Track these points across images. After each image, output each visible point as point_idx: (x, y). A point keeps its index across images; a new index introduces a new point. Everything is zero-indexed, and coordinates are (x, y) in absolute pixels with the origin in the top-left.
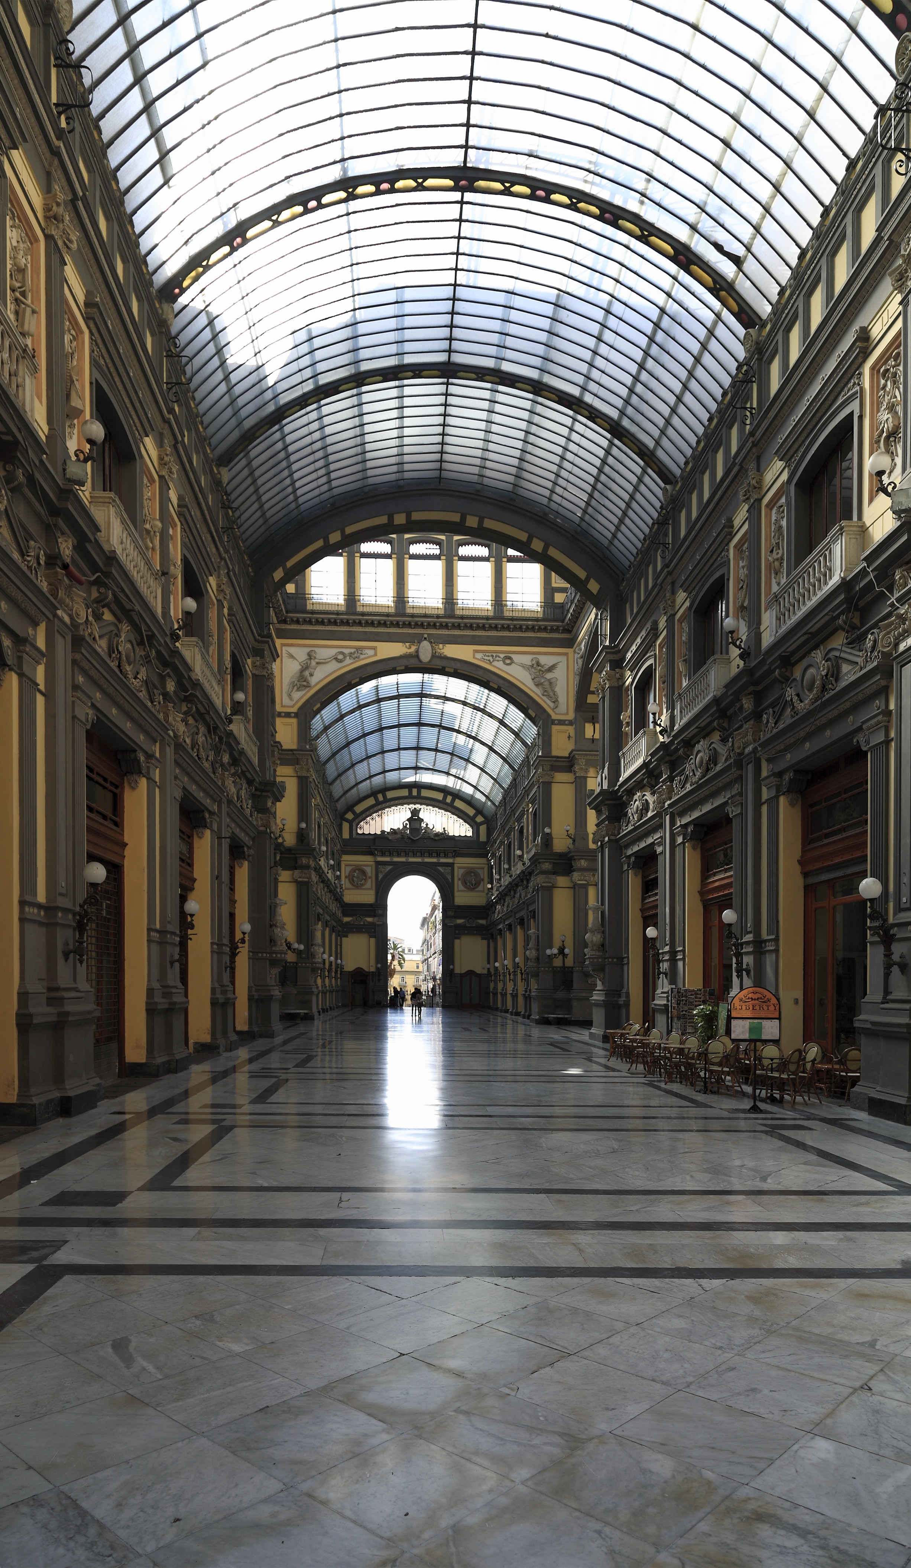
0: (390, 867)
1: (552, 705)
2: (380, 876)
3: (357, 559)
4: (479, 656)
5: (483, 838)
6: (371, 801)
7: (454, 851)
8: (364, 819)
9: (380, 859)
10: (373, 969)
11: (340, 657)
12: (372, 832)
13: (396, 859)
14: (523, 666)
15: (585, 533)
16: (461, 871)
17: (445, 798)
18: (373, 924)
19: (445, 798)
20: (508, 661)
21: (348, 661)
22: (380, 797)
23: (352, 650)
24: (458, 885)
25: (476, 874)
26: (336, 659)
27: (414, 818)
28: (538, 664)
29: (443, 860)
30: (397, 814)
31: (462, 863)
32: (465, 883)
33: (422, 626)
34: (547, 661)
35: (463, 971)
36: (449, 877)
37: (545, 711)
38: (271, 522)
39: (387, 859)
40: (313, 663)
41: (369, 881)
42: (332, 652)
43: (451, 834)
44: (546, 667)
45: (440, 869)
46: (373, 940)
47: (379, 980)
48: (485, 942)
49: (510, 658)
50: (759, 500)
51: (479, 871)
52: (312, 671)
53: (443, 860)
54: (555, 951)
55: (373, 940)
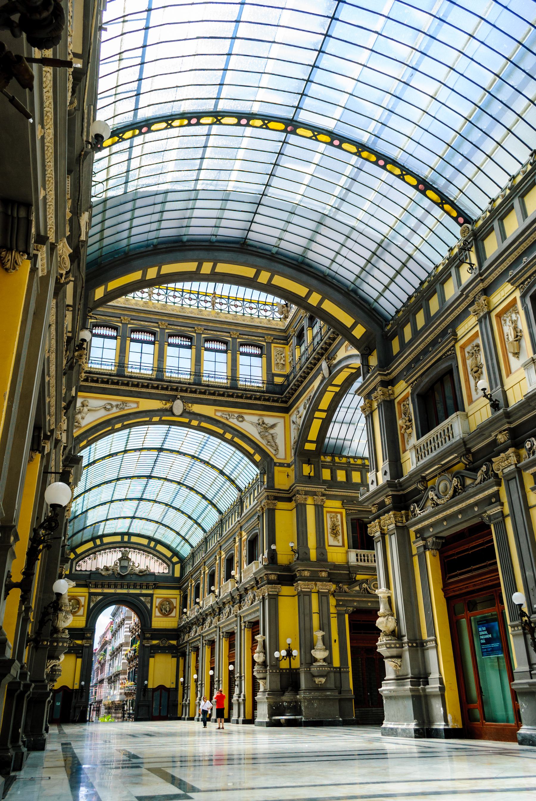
0: (100, 597)
1: (274, 452)
2: (92, 605)
3: (128, 342)
4: (219, 414)
5: (177, 574)
6: (91, 545)
7: (154, 584)
8: (88, 556)
9: (93, 590)
10: (76, 687)
11: (109, 407)
12: (88, 569)
13: (106, 591)
14: (252, 423)
15: (355, 291)
16: (159, 601)
17: (149, 543)
18: (82, 646)
19: (149, 543)
20: (241, 419)
21: (114, 410)
22: (98, 542)
23: (119, 403)
24: (156, 612)
25: (170, 603)
26: (105, 408)
27: (125, 558)
28: (263, 423)
29: (144, 592)
30: (110, 555)
31: (160, 595)
32: (161, 610)
33: (176, 390)
34: (269, 421)
35: (155, 686)
36: (149, 606)
37: (269, 456)
38: (106, 242)
39: (99, 591)
40: (85, 409)
41: (82, 609)
42: (102, 403)
43: (152, 571)
44: (269, 425)
45: (142, 598)
46: (79, 661)
47: (81, 697)
48: (175, 659)
49: (242, 417)
50: (489, 312)
51: (173, 600)
52: (84, 415)
53: (144, 592)
54: (284, 653)
55: (79, 661)
